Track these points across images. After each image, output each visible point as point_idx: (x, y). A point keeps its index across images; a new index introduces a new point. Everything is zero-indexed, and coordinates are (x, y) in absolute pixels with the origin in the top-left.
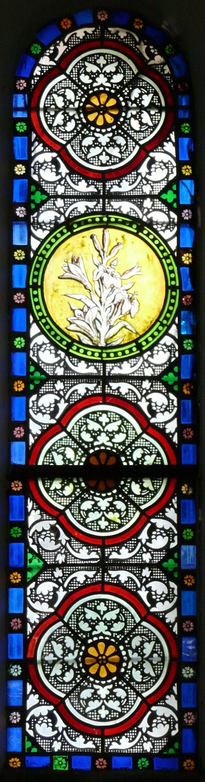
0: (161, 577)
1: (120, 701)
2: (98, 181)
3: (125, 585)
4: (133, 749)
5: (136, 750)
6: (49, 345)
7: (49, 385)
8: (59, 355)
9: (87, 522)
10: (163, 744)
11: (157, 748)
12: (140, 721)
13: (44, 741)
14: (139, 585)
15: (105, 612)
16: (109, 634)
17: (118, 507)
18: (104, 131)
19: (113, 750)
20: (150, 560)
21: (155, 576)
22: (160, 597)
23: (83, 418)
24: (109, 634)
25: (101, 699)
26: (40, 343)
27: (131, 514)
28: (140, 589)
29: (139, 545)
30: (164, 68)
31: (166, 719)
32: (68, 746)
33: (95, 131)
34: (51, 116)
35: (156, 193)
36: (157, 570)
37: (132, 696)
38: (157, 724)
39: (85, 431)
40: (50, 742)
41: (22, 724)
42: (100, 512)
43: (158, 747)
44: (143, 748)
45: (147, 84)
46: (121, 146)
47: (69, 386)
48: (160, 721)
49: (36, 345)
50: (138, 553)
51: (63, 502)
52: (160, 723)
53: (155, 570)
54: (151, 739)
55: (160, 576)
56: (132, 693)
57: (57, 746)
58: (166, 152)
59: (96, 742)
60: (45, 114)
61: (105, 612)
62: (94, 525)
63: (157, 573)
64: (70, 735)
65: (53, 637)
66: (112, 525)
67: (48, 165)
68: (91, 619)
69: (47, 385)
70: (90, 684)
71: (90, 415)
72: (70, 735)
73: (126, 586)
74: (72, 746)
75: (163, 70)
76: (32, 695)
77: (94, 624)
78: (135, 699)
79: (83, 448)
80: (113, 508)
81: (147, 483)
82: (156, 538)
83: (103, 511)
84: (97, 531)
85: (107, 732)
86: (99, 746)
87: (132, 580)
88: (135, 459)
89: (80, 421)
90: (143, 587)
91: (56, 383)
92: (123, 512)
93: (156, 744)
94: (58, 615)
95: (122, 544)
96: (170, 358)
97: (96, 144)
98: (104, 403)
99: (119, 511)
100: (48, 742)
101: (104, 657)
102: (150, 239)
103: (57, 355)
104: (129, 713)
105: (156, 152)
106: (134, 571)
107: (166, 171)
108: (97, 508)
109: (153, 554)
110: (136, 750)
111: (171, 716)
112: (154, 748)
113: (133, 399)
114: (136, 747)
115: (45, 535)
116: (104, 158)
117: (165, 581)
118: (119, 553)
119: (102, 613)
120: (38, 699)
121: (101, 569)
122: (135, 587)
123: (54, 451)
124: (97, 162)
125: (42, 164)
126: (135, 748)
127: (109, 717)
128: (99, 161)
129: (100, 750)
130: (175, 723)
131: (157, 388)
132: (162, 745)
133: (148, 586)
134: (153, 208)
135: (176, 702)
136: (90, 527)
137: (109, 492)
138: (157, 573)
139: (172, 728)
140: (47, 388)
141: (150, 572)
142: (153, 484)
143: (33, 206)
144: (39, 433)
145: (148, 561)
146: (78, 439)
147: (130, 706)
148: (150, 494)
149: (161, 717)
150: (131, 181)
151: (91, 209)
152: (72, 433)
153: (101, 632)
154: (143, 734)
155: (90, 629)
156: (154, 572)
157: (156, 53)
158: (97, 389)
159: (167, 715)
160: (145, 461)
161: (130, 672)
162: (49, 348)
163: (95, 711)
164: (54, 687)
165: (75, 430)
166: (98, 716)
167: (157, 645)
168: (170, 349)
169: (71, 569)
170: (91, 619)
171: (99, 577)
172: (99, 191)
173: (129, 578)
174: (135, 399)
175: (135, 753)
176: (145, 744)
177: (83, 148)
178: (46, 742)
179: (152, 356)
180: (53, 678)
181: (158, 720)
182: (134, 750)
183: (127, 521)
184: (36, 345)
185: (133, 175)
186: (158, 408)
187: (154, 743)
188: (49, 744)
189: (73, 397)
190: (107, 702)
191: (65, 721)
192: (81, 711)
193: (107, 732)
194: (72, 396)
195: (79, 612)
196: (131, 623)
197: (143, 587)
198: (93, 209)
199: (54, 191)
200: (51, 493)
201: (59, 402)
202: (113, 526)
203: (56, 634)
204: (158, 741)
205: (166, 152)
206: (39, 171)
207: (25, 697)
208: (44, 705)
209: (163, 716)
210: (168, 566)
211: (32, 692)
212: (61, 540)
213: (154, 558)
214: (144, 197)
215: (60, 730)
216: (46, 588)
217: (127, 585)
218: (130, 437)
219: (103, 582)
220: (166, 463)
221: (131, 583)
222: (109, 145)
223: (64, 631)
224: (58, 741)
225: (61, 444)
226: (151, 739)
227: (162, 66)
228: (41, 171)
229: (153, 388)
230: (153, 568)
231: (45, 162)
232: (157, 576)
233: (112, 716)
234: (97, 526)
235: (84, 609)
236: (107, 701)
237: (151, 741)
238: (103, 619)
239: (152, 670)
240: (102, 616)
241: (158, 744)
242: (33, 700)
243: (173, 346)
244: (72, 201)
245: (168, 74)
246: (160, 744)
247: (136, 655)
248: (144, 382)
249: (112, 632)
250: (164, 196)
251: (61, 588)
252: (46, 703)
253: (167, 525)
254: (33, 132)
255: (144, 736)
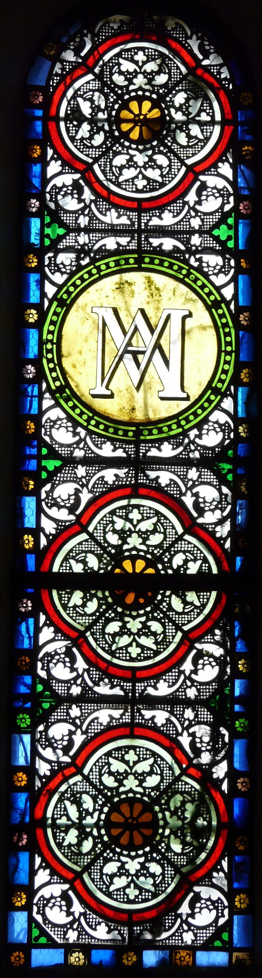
0: (212, 480)
1: (161, 170)
2: (123, 924)
3: (166, 489)
4: (169, 940)
5: (182, 226)
6: (65, 421)
7: (62, 711)
8: (78, 434)
9: (120, 180)
10: (211, 690)
11: (207, 225)
12: (179, 904)
13: (56, 929)
14: (180, 729)
15: (135, 763)
16: (144, 548)
17: (159, 163)
18: (134, 552)
19: (153, 226)
20: (200, 226)
21: (204, 478)
22: (213, 269)
23: (108, 515)
24: (144, 548)
25: (138, 166)
26: (54, 418)
27: (168, 880)
28: (185, 494)
29: (182, 677)
30: (221, 71)
31: (219, 191)
32: (97, 222)
33: (129, 148)
34: (74, 126)
35: (207, 227)
36: (207, 472)
37: (170, 631)
38: (207, 196)
39: (112, 531)
40: (75, 217)
41: (28, 908)
42: (136, 168)
43: (208, 223)
44: (190, 225)
45: (194, 547)
46: (163, 168)
47: (95, 240)
48: (205, 905)
49: (48, 421)
50: (180, 687)
51: (92, 154)
52: (207, 664)
53: (204, 472)
54: (192, 928)
55: (210, 478)
56: (170, 627)
57: (72, 936)
58: (220, 175)
59: (131, 217)
60: (66, 124)
61: (135, 763)
62: (122, 653)
63: (207, 475)
64: (93, 677)
65: (71, 554)
66: (145, 652)
67: (56, 901)
68: (127, 71)
69: (59, 711)
70: (116, 856)
71: (118, 511)
72: (100, 208)
73: (167, 490)
74: (101, 221)
75: (219, 73)
76: (42, 870)
77: (131, 76)
78: (174, 634)
79: (105, 796)
80: (153, 164)
81: (191, 596)
82: (206, 200)
83: (140, 167)
84: (132, 192)
85: (145, 205)
86: (135, 222)
87: (175, 483)
88: (175, 567)
89: (105, 519)
90: (189, 492)
91: (79, 235)
92: (166, 168)
93: (198, 935)
94: (76, 766)
95: (160, 677)
96: (224, 440)
97: (130, 163)
98: (132, 736)
99: (160, 167)
100: (65, 686)
101: (142, 117)
102: (198, 286)
103: (75, 434)
104: (166, 651)
105: (208, 175)
106: (177, 472)
107: (220, 200)
108: (133, 163)
109: (197, 933)
110: (173, 941)
111: (225, 187)
112: (196, 940)
113: (175, 492)
114: (182, 223)
115: (60, 425)
116: (132, 893)
117: (216, 485)
118: (161, 219)
119: (131, 764)
120: (49, 875)
121: (129, 707)
122: (178, 492)
123: (72, 558)
124: (122, 896)
125: (48, 900)
126: (172, 939)
127: (141, 657)
128: (134, 186)
129: (136, 226)
130: (229, 195)
131: (207, 478)
132: (213, 222)
133: (194, 491)
134: (200, 480)
135: (231, 171)
136: (124, 187)
137: (141, 610)
138: (207, 475)
139: (220, 915)
140: (59, 714)
141: (198, 473)
142: (199, 598)
143: (44, 475)
144: (52, 629)
145: (197, 228)
146: (102, 541)
147: (173, 176)
148: (199, 144)
149: (213, 188)
150: (171, 681)
151: (123, 246)
152: (95, 534)
153: (134, 620)
154: (190, 208)
155: (116, 784)
156: (203, 473)
157: (212, 51)
158: (124, 717)
159: (220, 187)
160: (187, 568)
161: (168, 599)
162: (65, 425)
163: (122, 890)
164: (80, 151)
165: (99, 531)
166: (128, 655)
167: (204, 565)
168: (223, 427)
169: (91, 706)
170: (127, 71)
171: (127, 717)
172: (133, 224)
173: (171, 480)
174: (174, 732)
175: (172, 945)
176: (192, 220)
177: (104, 877)
178: (62, 686)
179: (200, 436)
180: (71, 609)
181: (208, 192)
182: (179, 227)
183: (170, 179)
184: (42, 899)
185: (174, 674)
186: (211, 269)
187: (204, 219)
188: (66, 688)
189: (93, 727)
190: (146, 170)
191: (87, 660)
192: (104, 890)
193: (135, 918)
194: (91, 726)
195: (106, 521)
196: (172, 535)
197: (189, 492)
198: (125, 246)
199: (75, 223)
200: (77, 143)
201: (74, 733)
202: (147, 653)
203: (76, 550)
204: (204, 687)
205: (220, 175)
206: (50, 431)
207: (33, 873)
208: (68, 173)
209: (209, 899)
210: (217, 704)
211: (40, 867)
212: (74, 912)
213: (205, 223)
214: (192, 232)
215: (80, 672)
216: (64, 491)
217: (169, 489)
218: (169, 538)
219: (134, 680)
220: (215, 571)
221: (174, 487)
222: (147, 166)
223: (85, 547)
224: (74, 930)
225: (88, 88)
226: (195, 684)
227: (213, 526)
228: (53, 430)
229: (201, 479)
230: (201, 469)
231: (52, 897)
232: (207, 478)
233: (146, 655)
234: (132, 185)
235: (112, 517)
236: (146, 169)
237: (193, 931)
238: (142, 71)
239: (196, 597)
240: (140, 68)
241: (205, 691)
242: (47, 634)
243: (227, 425)
244: (99, 237)
245: (225, 79)
246: (207, 690)
247: (180, 113)
248: (192, 236)
249: (144, 788)
250: (216, 232)
251: (79, 730)
252: (63, 638)
253: (221, 183)
254: (41, 613)
255: (184, 925)
